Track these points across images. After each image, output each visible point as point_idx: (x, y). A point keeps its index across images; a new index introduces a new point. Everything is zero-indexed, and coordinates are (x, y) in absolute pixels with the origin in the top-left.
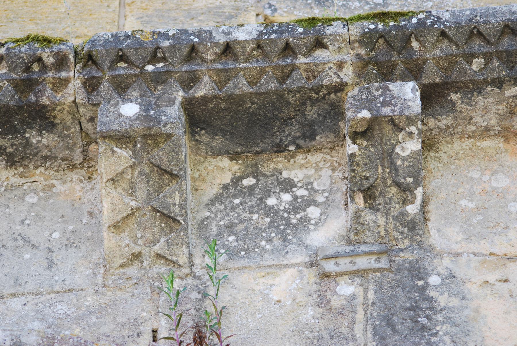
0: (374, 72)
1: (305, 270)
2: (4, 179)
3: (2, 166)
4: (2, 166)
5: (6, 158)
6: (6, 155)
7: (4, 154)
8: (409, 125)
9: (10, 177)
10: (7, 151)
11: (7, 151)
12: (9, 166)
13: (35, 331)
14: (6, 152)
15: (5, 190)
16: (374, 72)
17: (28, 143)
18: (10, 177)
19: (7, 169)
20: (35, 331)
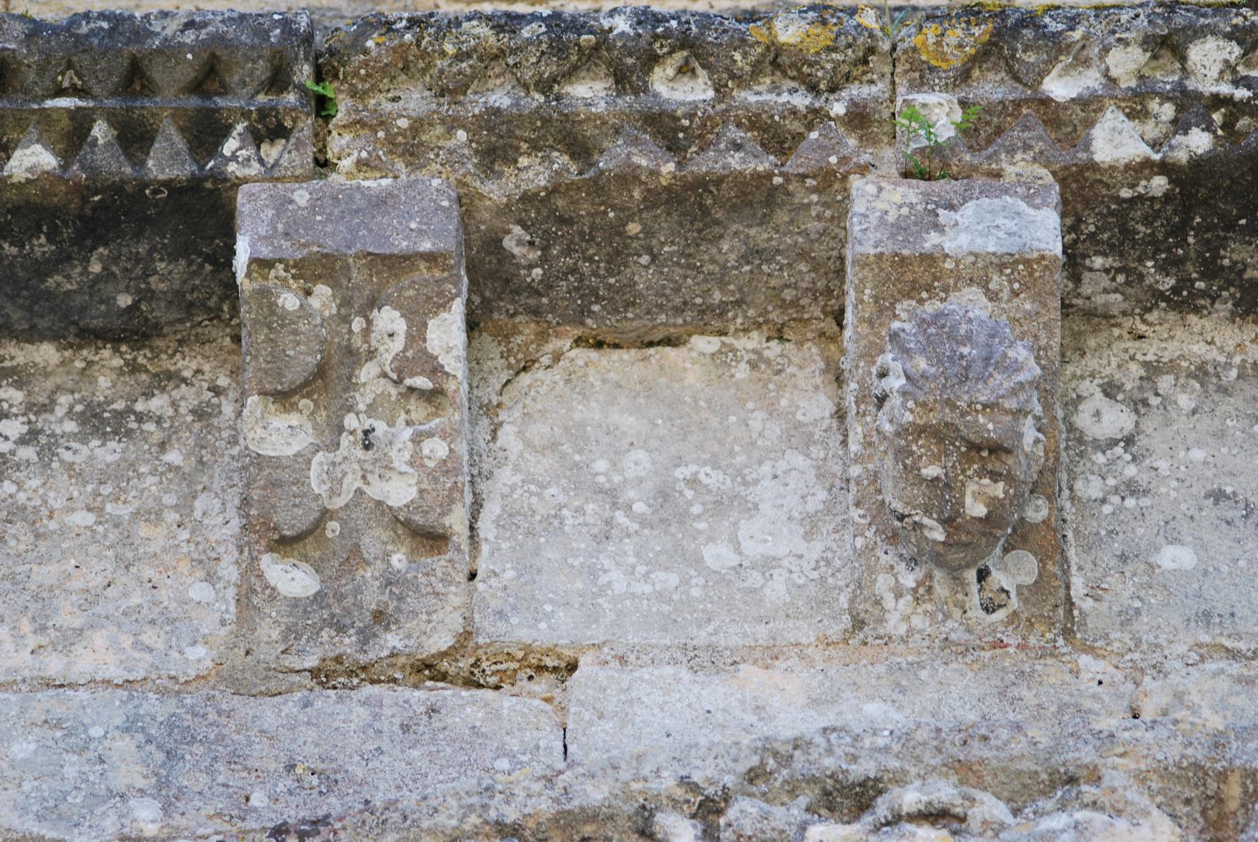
0: (445, 203)
1: (1126, 703)
2: (1232, 348)
3: (1222, 314)
4: (1222, 314)
5: (1238, 295)
6: (1241, 287)
7: (1237, 283)
8: (427, 281)
9: (1247, 343)
10: (1246, 276)
11: (1246, 276)
12: (1240, 316)
13: (1063, 831)
14: (1242, 279)
15: (1239, 377)
16: (445, 203)
17: (393, 164)
18: (1247, 343)
19: (1234, 322)
20: (1063, 831)
